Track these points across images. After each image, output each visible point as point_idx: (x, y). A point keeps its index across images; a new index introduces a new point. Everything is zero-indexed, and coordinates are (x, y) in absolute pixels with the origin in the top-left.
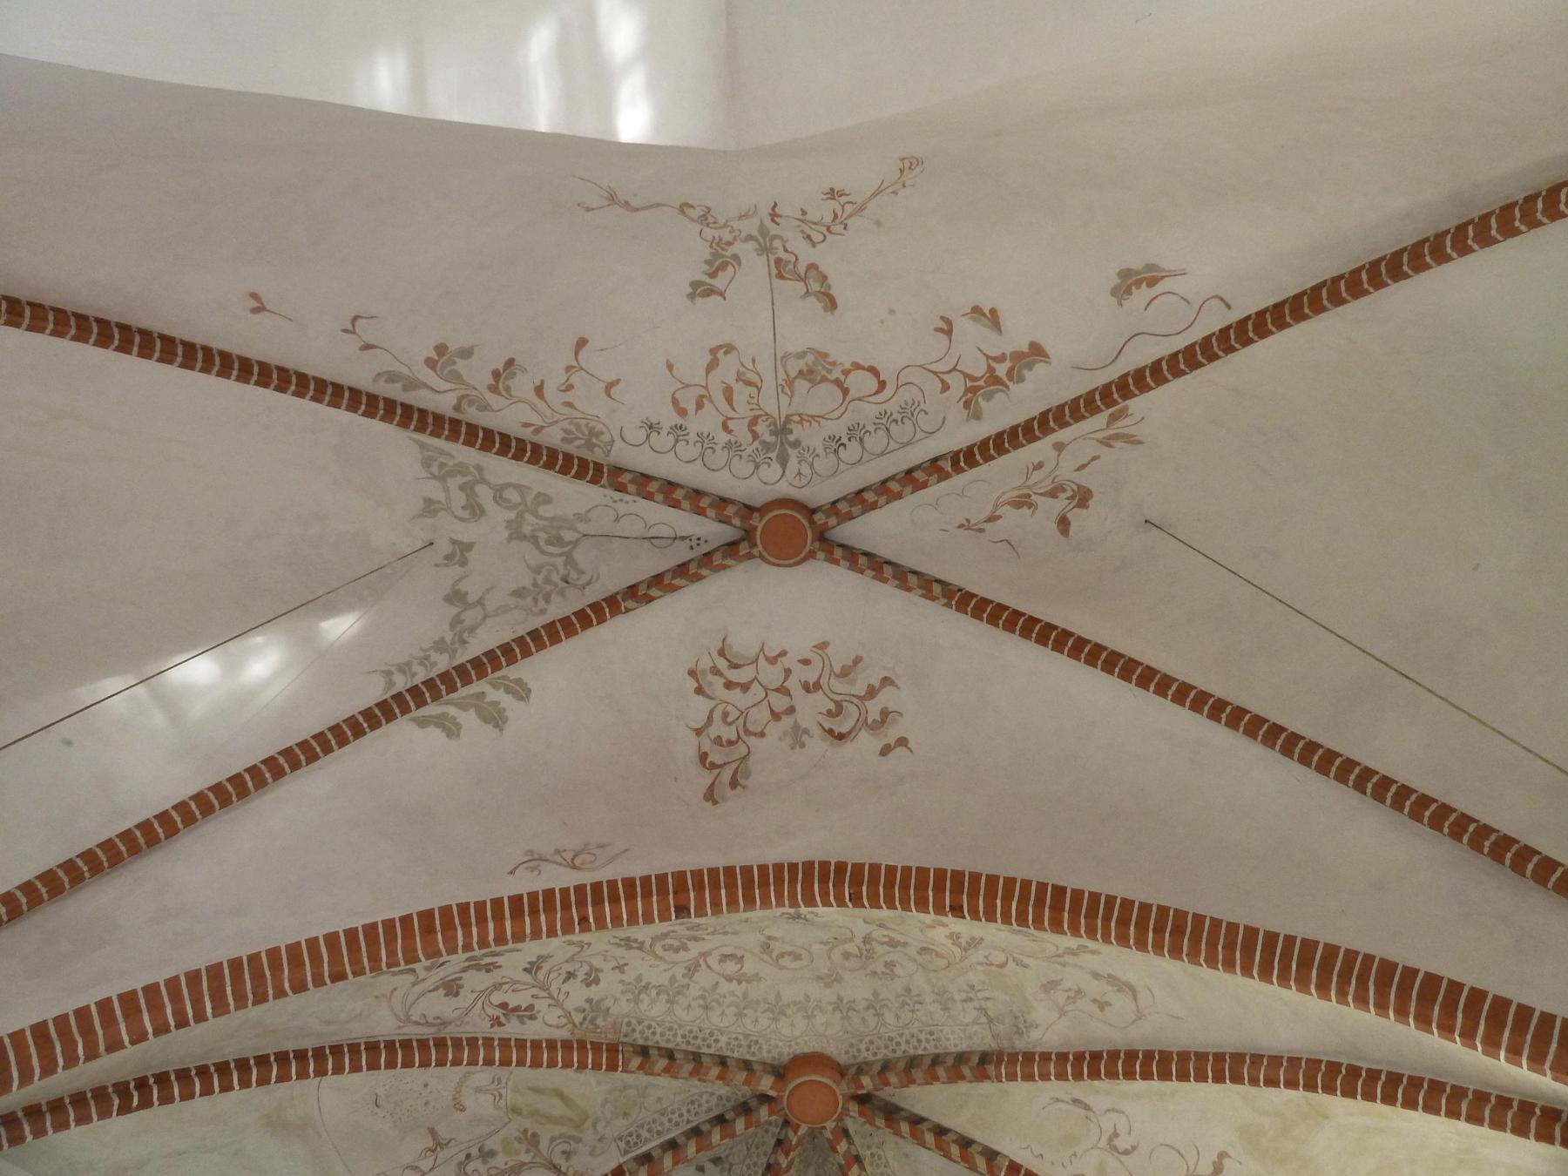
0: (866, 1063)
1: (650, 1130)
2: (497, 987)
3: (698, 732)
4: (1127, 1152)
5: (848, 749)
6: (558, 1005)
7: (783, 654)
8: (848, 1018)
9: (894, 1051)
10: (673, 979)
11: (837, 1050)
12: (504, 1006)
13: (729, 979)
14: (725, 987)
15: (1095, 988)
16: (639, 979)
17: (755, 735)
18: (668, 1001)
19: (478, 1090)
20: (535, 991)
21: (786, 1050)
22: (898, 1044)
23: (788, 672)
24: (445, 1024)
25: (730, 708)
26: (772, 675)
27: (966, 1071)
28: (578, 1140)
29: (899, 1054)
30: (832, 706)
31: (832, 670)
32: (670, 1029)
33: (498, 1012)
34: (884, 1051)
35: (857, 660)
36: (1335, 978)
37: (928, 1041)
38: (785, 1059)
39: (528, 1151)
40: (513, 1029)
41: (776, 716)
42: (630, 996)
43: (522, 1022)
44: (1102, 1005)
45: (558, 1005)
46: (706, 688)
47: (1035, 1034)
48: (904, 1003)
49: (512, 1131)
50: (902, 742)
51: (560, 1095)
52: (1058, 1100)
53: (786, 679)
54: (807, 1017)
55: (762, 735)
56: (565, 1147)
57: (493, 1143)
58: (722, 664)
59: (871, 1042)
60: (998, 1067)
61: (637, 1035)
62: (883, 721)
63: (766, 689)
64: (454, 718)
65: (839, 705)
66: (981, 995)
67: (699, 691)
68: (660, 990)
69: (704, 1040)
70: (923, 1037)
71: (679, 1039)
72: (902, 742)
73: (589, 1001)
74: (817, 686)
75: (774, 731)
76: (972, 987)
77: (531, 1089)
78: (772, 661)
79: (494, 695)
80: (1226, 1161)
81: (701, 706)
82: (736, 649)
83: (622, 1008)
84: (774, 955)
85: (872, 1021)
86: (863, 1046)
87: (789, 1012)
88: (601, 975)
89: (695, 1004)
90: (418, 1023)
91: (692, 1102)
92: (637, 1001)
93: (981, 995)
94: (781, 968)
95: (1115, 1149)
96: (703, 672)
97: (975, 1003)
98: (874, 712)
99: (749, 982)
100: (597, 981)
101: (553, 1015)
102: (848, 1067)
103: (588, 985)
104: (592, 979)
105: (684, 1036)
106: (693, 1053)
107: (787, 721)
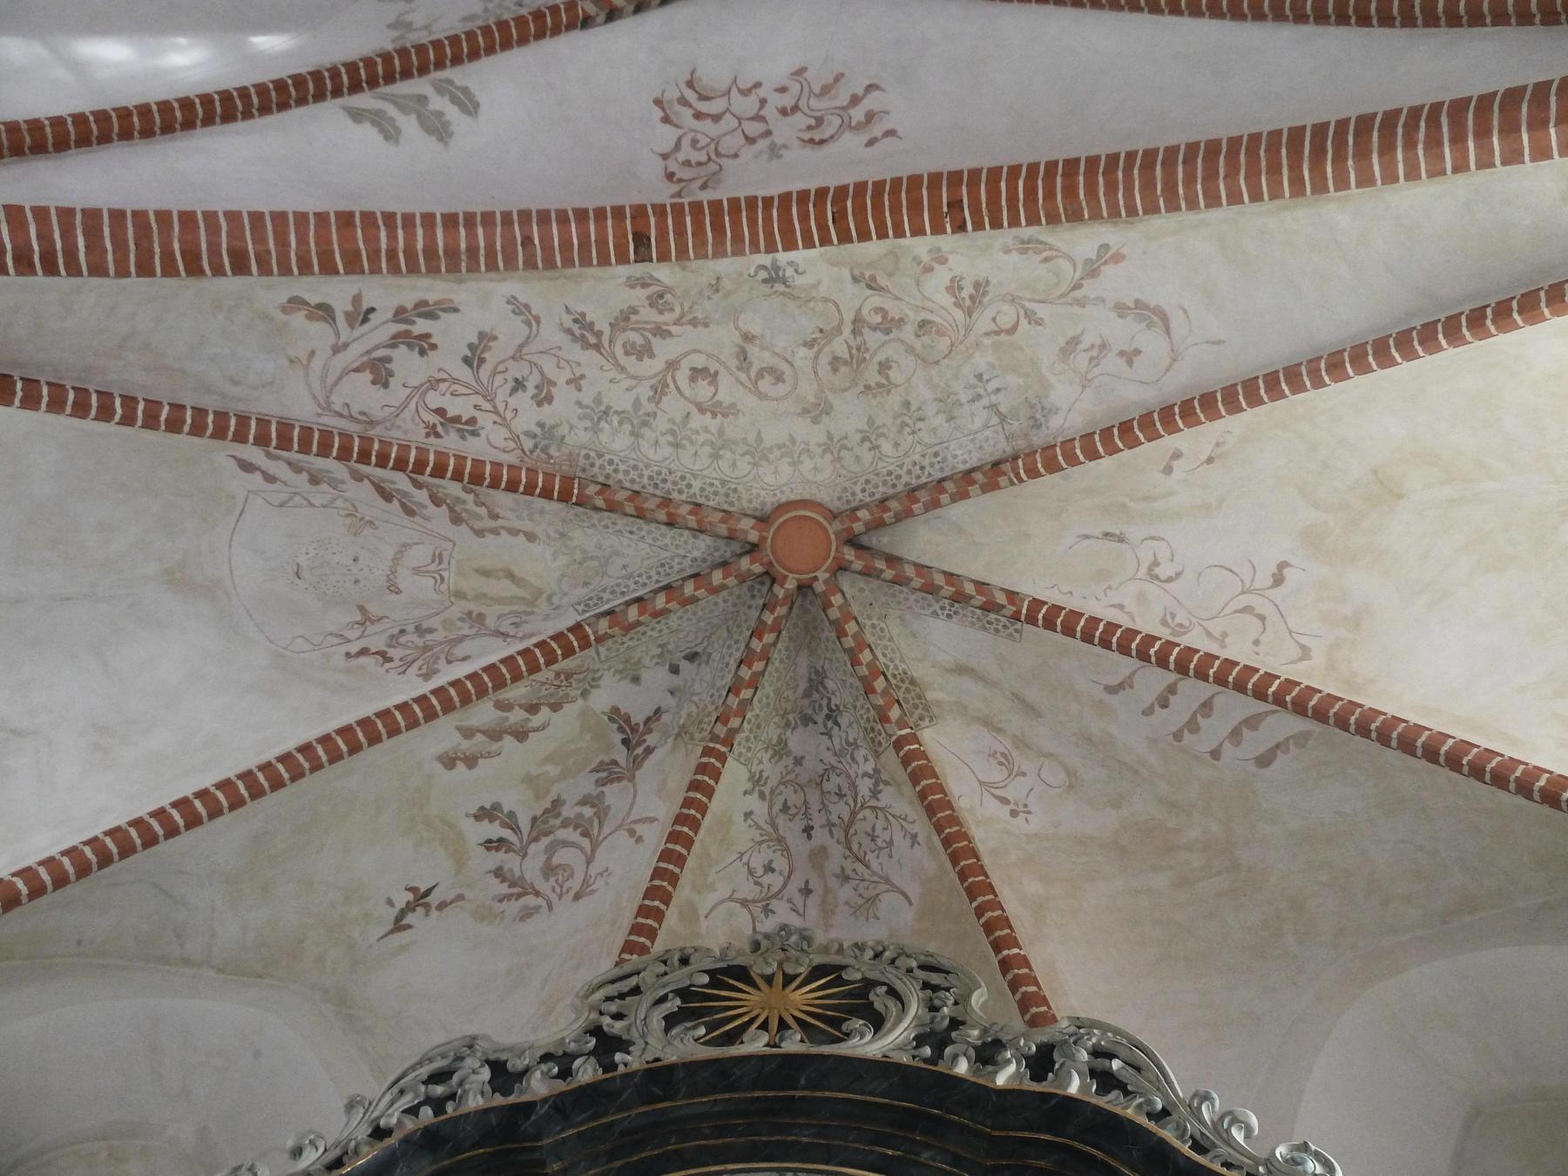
2: (433, 384)
4: (1170, 580)
6: (505, 424)
7: (758, 85)
8: (840, 459)
9: (894, 486)
10: (637, 403)
11: (823, 497)
12: (441, 412)
13: (702, 410)
14: (697, 421)
15: (1121, 331)
16: (598, 400)
18: (632, 433)
19: (417, 571)
20: (478, 400)
21: (769, 500)
22: (899, 477)
23: (763, 102)
24: (372, 423)
25: (699, 136)
28: (531, 613)
30: (813, 122)
31: (811, 91)
32: (635, 468)
33: (434, 419)
34: (882, 489)
36: (1400, 131)
37: (932, 465)
38: (769, 508)
40: (451, 442)
42: (588, 424)
43: (463, 438)
44: (1130, 356)
45: (505, 424)
46: (672, 117)
47: (1055, 422)
48: (904, 425)
49: (456, 611)
50: (891, 133)
51: (511, 576)
52: (1087, 537)
54: (793, 464)
57: (435, 622)
58: (691, 95)
59: (868, 482)
61: (596, 470)
63: (739, 119)
64: (392, 120)
66: (991, 387)
67: (666, 120)
68: (623, 417)
69: (675, 483)
70: (926, 462)
71: (645, 481)
73: (541, 425)
76: (980, 377)
77: (477, 571)
78: (745, 93)
79: (438, 103)
80: (1286, 571)
81: (669, 135)
82: (705, 81)
83: (579, 437)
84: (753, 372)
85: (867, 457)
86: (858, 489)
87: (771, 457)
88: (554, 390)
89: (663, 440)
90: (341, 415)
91: (663, 565)
92: (596, 430)
93: (991, 387)
94: (762, 396)
95: (1157, 577)
97: (985, 402)
98: (858, 114)
99: (725, 415)
100: (549, 399)
101: (499, 436)
103: (540, 404)
104: (544, 398)
105: (651, 478)
107: (763, 144)
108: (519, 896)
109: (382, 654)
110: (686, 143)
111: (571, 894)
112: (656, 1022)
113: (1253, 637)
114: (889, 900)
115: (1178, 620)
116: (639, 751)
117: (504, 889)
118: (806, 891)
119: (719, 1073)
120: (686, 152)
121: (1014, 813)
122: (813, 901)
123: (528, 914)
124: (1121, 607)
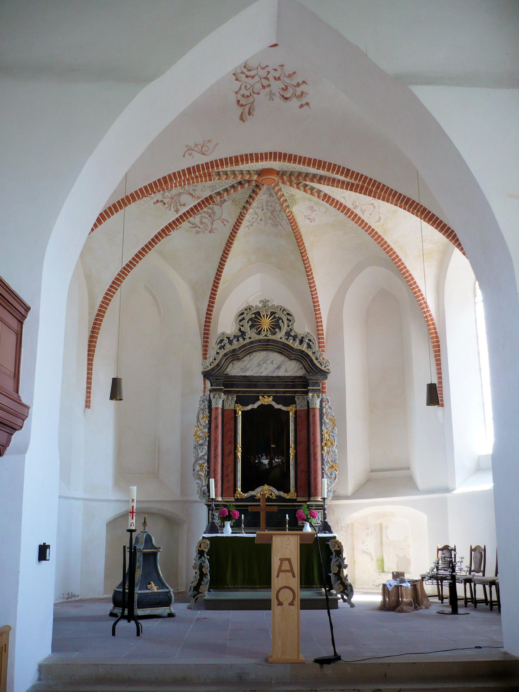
0: (285, 171)
1: (219, 185)
3: (236, 93)
5: (289, 103)
7: (267, 66)
17: (256, 93)
23: (269, 72)
26: (263, 73)
27: (315, 180)
29: (296, 170)
30: (284, 87)
31: (285, 74)
35: (294, 73)
38: (261, 169)
39: (182, 189)
41: (264, 87)
53: (268, 75)
55: (259, 93)
56: (193, 188)
58: (245, 70)
60: (325, 181)
62: (301, 96)
63: (260, 78)
65: (286, 87)
67: (237, 79)
72: (307, 104)
74: (279, 79)
75: (264, 92)
78: (263, 68)
86: (285, 167)
96: (238, 74)
102: (279, 171)
106: (233, 171)
107: (267, 89)
108: (195, 228)
109: (162, 201)
110: (243, 87)
111: (208, 231)
112: (249, 329)
113: (370, 212)
114: (279, 227)
115: (356, 204)
116: (222, 199)
117: (191, 225)
118: (261, 220)
119: (259, 341)
120: (243, 91)
121: (311, 222)
122: (263, 222)
123: (198, 232)
124: (344, 198)
